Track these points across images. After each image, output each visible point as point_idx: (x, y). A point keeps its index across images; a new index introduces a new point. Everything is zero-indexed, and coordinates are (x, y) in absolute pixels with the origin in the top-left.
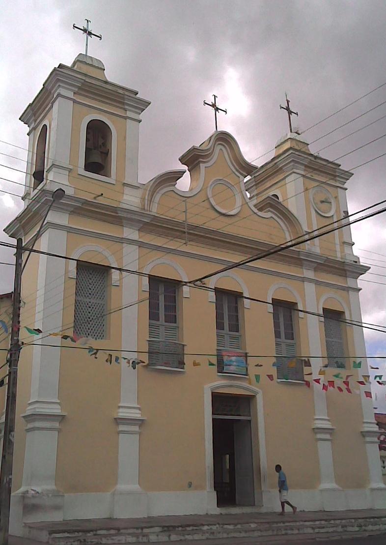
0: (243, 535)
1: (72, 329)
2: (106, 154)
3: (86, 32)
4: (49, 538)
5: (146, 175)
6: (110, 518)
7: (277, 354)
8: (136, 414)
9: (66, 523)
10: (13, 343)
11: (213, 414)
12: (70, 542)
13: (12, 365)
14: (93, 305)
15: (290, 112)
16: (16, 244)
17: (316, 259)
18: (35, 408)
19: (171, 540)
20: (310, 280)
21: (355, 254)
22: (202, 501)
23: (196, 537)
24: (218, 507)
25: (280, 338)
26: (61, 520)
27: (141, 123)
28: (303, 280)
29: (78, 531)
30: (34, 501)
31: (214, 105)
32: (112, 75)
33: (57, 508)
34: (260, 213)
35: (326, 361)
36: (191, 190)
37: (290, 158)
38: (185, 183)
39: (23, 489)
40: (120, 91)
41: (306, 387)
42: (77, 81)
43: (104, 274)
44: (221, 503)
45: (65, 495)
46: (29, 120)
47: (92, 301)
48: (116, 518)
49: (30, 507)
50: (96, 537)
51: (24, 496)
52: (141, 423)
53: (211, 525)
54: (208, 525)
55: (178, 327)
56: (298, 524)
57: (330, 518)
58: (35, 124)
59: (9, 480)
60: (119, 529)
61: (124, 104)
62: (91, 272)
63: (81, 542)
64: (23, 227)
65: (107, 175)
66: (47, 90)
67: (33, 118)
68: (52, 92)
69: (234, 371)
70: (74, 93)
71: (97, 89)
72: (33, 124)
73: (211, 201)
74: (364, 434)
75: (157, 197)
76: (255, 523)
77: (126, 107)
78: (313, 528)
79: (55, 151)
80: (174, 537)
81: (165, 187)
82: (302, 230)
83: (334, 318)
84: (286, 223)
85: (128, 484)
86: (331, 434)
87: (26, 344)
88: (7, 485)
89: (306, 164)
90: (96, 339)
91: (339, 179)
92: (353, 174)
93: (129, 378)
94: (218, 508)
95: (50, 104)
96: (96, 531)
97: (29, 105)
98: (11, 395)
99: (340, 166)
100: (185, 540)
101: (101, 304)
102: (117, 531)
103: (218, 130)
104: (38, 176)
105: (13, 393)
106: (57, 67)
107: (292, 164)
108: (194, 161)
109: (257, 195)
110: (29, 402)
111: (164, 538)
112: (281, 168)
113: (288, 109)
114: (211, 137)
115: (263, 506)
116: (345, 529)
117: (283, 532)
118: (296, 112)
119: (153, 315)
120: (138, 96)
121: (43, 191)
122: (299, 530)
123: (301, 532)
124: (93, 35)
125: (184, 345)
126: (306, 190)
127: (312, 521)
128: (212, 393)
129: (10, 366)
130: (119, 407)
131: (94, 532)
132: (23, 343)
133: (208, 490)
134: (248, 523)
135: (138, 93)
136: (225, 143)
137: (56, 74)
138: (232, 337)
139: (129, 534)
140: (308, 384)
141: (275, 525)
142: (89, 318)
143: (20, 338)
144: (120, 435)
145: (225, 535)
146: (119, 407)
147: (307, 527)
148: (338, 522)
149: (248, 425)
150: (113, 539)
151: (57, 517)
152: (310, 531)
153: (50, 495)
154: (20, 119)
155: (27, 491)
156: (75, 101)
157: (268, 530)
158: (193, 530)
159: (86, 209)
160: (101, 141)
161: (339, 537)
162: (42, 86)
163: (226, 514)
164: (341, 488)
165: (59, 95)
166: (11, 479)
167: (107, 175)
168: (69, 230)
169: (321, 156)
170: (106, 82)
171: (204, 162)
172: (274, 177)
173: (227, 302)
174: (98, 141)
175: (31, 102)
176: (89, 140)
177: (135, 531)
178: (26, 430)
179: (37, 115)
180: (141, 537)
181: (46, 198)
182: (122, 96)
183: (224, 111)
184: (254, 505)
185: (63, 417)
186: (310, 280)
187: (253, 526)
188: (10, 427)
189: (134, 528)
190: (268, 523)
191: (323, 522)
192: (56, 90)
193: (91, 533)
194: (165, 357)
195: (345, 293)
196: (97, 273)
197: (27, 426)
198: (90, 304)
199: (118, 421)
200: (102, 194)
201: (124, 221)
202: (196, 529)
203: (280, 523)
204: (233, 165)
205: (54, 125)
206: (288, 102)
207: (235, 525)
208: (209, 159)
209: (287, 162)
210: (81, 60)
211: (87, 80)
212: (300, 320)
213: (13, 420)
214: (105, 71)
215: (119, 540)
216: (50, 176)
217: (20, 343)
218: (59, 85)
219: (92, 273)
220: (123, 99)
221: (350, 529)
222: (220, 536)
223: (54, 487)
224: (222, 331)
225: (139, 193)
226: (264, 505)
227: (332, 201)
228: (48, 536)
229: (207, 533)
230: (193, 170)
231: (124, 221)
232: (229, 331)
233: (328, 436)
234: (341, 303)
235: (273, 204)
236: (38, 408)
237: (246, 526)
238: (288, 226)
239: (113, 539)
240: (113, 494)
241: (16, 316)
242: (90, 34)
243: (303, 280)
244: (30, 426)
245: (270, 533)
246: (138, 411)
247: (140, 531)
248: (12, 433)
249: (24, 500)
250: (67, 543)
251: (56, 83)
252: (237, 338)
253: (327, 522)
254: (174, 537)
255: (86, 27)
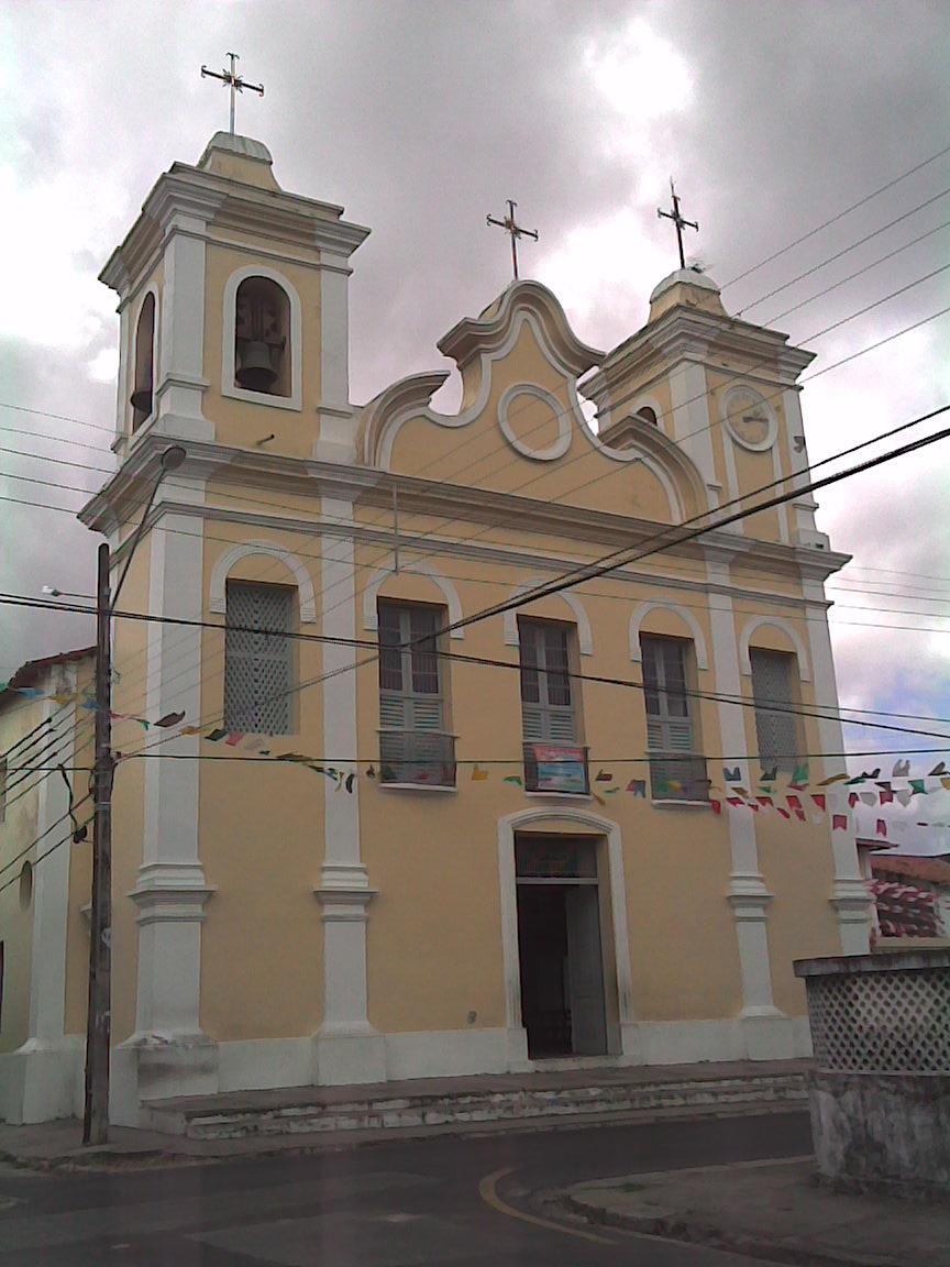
0: (572, 1109)
1: (222, 722)
2: (280, 347)
3: (230, 81)
4: (187, 1127)
5: (365, 384)
6: (312, 1086)
7: (650, 747)
8: (359, 882)
9: (222, 1097)
10: (100, 755)
11: (517, 876)
12: (227, 1132)
13: (100, 798)
14: (264, 663)
15: (680, 224)
16: (96, 606)
17: (726, 544)
18: (152, 879)
19: (427, 1122)
20: (722, 590)
21: (820, 529)
22: (500, 1048)
23: (477, 1116)
24: (530, 1057)
25: (659, 714)
26: (215, 1093)
27: (352, 275)
28: (707, 589)
29: (244, 1112)
30: (163, 1059)
31: (509, 224)
32: (288, 179)
33: (205, 1070)
34: (607, 450)
35: (639, 794)
36: (463, 410)
37: (678, 327)
38: (446, 402)
39: (136, 1037)
40: (306, 211)
41: (712, 812)
42: (208, 196)
43: (283, 599)
44: (533, 1053)
45: (221, 1044)
46: (118, 279)
47: (260, 656)
48: (324, 1086)
49: (150, 1069)
50: (277, 1121)
51: (139, 1049)
52: (368, 898)
53: (508, 1093)
54: (503, 1093)
55: (442, 701)
56: (685, 1086)
57: (751, 1073)
58: (131, 288)
59: (105, 1021)
60: (324, 1106)
61: (312, 237)
62: (256, 597)
63: (248, 1131)
64: (117, 508)
65: (284, 392)
66: (150, 218)
67: (126, 277)
68: (161, 224)
69: (561, 786)
70: (208, 223)
71: (259, 212)
72: (127, 289)
73: (504, 430)
74: (837, 904)
75: (390, 434)
76: (600, 1087)
77: (319, 244)
78: (714, 1094)
79: (177, 352)
80: (432, 1118)
81: (402, 412)
82: (701, 480)
83: (773, 663)
84: (671, 474)
85: (346, 1017)
86: (765, 907)
87: (126, 755)
88: (102, 1029)
89: (712, 339)
90: (271, 734)
91: (783, 367)
92: (815, 355)
93: (342, 813)
94: (531, 1062)
95: (158, 251)
96: (279, 1109)
97: (116, 252)
98: (100, 857)
99: (788, 337)
100: (456, 1122)
101: (275, 661)
102: (320, 1109)
103: (522, 277)
104: (142, 402)
105: (104, 853)
106: (167, 170)
107: (682, 340)
108: (471, 348)
109: (612, 408)
110: (142, 867)
111: (413, 1119)
112: (659, 351)
113: (675, 215)
114: (503, 296)
115: (622, 1053)
116: (782, 1094)
117: (654, 1103)
118: (692, 222)
119: (389, 679)
120: (342, 218)
121: (151, 439)
122: (685, 1098)
123: (689, 1101)
124: (245, 85)
125: (454, 738)
126: (712, 392)
127: (714, 1080)
128: (515, 832)
129: (95, 800)
130: (324, 869)
131: (276, 1112)
132: (119, 753)
133: (509, 1026)
134: (583, 1088)
135: (342, 213)
136: (532, 304)
137: (167, 186)
138: (556, 716)
139: (342, 1114)
140: (716, 806)
141: (639, 1090)
142: (256, 692)
143: (113, 745)
144: (328, 925)
145: (536, 1112)
146: (324, 869)
147: (701, 1091)
148: (770, 1081)
149: (592, 896)
150: (311, 1125)
151: (204, 1087)
152: (708, 1099)
153: (191, 1047)
154: (99, 279)
155: (145, 1041)
156: (209, 241)
157: (624, 1099)
158: (472, 1102)
159: (241, 468)
160: (268, 321)
161: (765, 1111)
162: (140, 212)
163: (548, 1073)
164: (783, 1015)
165: (175, 230)
166: (109, 1017)
167: (284, 392)
168: (209, 515)
169: (743, 318)
170: (276, 193)
171: (488, 351)
172: (629, 381)
173: (543, 642)
174: (262, 338)
175: (120, 244)
176: (243, 322)
177: (358, 1108)
178: (138, 922)
179: (133, 272)
180: (366, 1119)
181: (156, 452)
182: (310, 221)
183: (532, 235)
184: (606, 1053)
185: (210, 893)
186: (722, 590)
187: (593, 1092)
188: (102, 919)
189: (355, 1102)
190: (625, 1086)
191: (737, 1082)
192: (170, 218)
193: (270, 1113)
194: (415, 764)
195: (796, 613)
196: (268, 599)
197: (139, 914)
198: (257, 663)
199: (322, 897)
200: (273, 437)
201: (323, 488)
202: (478, 1102)
203: (649, 1084)
204: (553, 353)
205: (168, 291)
206: (676, 200)
207: (558, 1091)
208: (497, 345)
209: (672, 337)
210: (224, 146)
211: (231, 195)
212: (700, 674)
213: (107, 905)
214: (273, 167)
215: (323, 1126)
216: (165, 406)
217: (113, 754)
218: (175, 209)
219: (258, 609)
220: (313, 227)
221: (791, 1094)
222: (526, 1112)
223: (197, 1031)
224: (534, 705)
225: (354, 424)
226: (625, 1053)
227: (770, 416)
228: (185, 1123)
229: (500, 1108)
230: (469, 367)
231: (323, 488)
232: (550, 703)
233: (759, 912)
234: (789, 636)
235: (641, 431)
236: (159, 878)
237: (579, 1093)
238: (671, 474)
239: (311, 1125)
240: (317, 1040)
241: (103, 698)
242: (238, 84)
243: (707, 589)
244: (145, 913)
245: (627, 1104)
246: (362, 876)
247: (366, 1107)
248: (107, 931)
249: (138, 1057)
250: (220, 1134)
251: (166, 206)
252: (566, 718)
253: (745, 1083)
254: (432, 1118)
255: (229, 70)
